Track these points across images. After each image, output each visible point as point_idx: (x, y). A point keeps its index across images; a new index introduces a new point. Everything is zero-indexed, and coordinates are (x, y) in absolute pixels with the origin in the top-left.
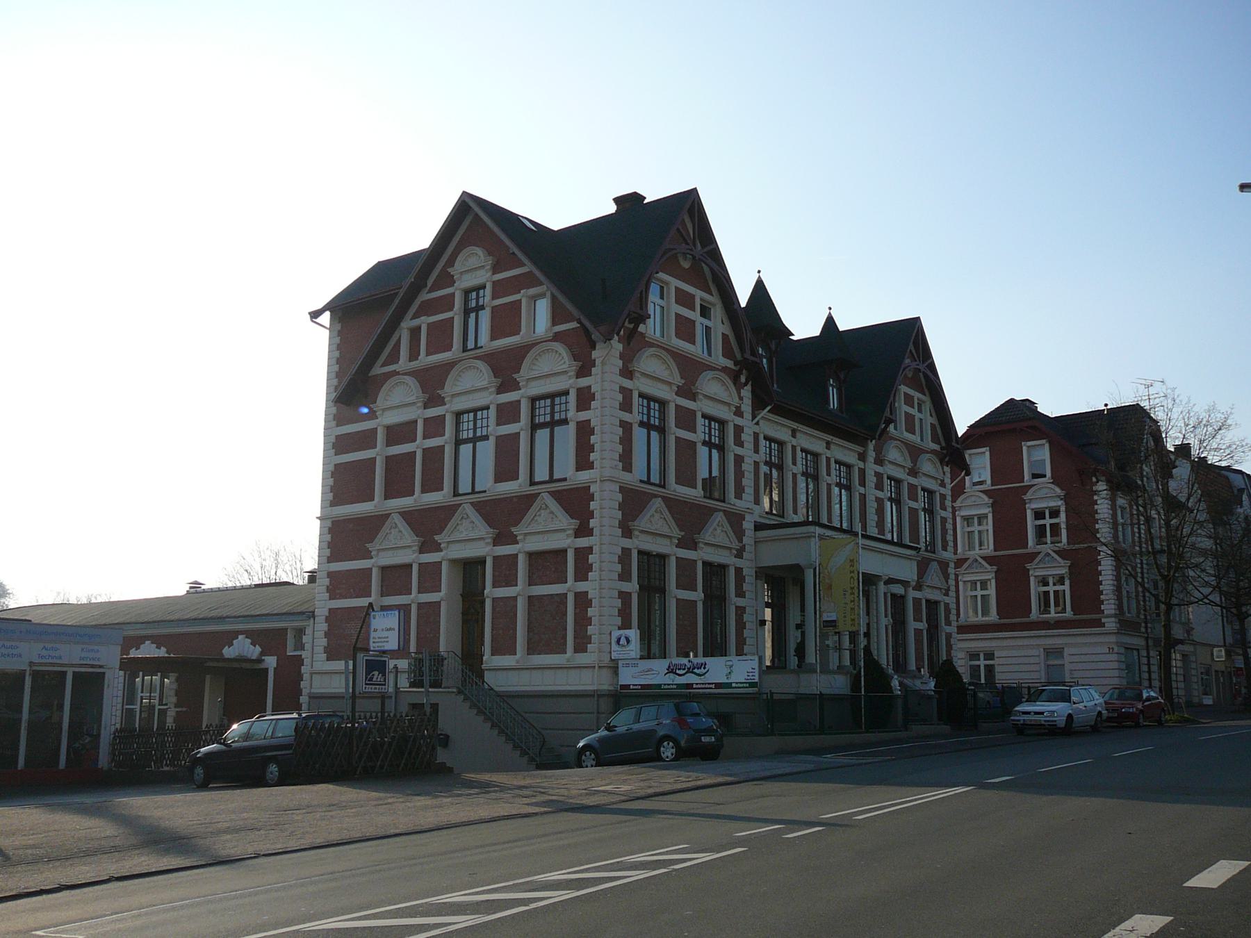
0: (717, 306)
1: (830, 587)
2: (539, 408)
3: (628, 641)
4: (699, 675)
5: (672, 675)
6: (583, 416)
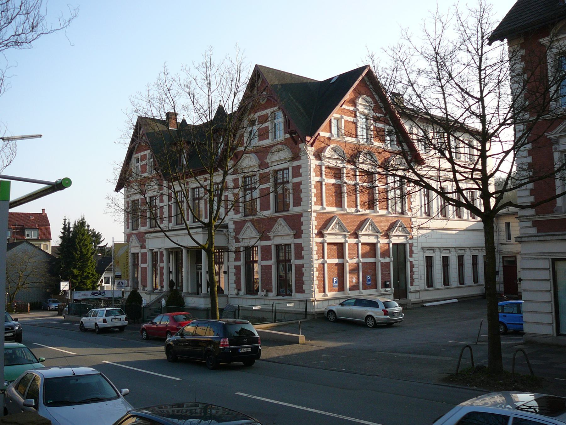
0: (352, 308)
1: (118, 262)
3: (122, 283)
4: (102, 295)
5: (93, 296)
6: (296, 180)
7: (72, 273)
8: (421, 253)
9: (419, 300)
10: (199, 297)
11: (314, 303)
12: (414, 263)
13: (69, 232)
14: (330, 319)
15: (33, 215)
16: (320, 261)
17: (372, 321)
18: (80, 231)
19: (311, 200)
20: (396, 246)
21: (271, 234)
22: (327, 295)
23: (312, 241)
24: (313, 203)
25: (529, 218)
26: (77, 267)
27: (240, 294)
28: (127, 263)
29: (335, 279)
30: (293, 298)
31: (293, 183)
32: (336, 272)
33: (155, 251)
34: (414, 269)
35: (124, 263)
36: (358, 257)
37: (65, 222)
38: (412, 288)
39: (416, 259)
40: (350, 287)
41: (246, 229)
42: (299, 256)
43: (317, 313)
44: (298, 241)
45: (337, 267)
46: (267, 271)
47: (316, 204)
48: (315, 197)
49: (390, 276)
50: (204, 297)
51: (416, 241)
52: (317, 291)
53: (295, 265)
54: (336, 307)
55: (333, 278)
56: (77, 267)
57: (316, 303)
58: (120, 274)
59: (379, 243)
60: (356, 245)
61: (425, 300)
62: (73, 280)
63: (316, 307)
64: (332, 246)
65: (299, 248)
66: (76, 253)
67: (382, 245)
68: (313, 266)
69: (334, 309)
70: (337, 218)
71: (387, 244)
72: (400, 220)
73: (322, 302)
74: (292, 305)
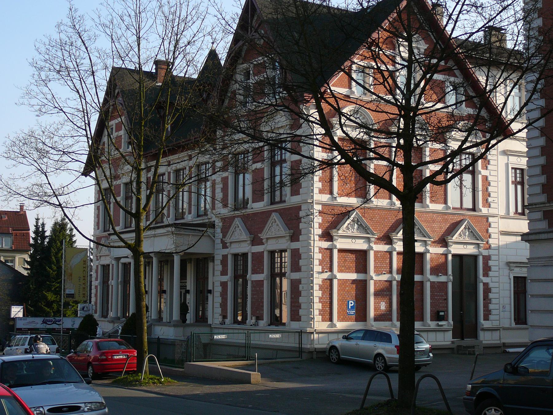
0: (358, 343)
1: (71, 275)
2: (285, 257)
5: (45, 324)
7: (45, 298)
8: (506, 271)
9: (499, 342)
10: (169, 326)
11: (312, 335)
12: (491, 285)
13: (43, 237)
14: (378, 367)
15: (6, 214)
16: (326, 275)
17: (383, 363)
18: (59, 237)
19: (313, 186)
20: (458, 259)
21: (263, 236)
22: (335, 326)
23: (312, 245)
24: (316, 191)
25: (538, 206)
26: (53, 289)
27: (226, 324)
28: (84, 277)
29: (352, 303)
30: (287, 328)
31: (292, 162)
32: (353, 293)
33: (123, 261)
34: (491, 296)
35: (80, 278)
36: (391, 272)
37: (37, 223)
38: (486, 324)
39: (494, 279)
40: (375, 315)
41: (235, 229)
42: (296, 267)
43: (317, 350)
44: (295, 245)
45: (354, 286)
46: (258, 289)
47: (321, 192)
48: (320, 181)
49: (447, 303)
50: (175, 326)
51: (496, 252)
52: (318, 318)
53: (291, 280)
54: (339, 343)
55: (348, 301)
56: (53, 289)
57: (316, 336)
58: (73, 293)
59: (429, 252)
60: (388, 254)
61: (508, 343)
62: (46, 308)
63: (316, 342)
64: (347, 254)
65: (296, 255)
66: (51, 268)
67: (434, 256)
68: (312, 282)
69: (337, 344)
70: (355, 213)
71: (442, 254)
72: (466, 220)
73: (327, 335)
74: (278, 336)
